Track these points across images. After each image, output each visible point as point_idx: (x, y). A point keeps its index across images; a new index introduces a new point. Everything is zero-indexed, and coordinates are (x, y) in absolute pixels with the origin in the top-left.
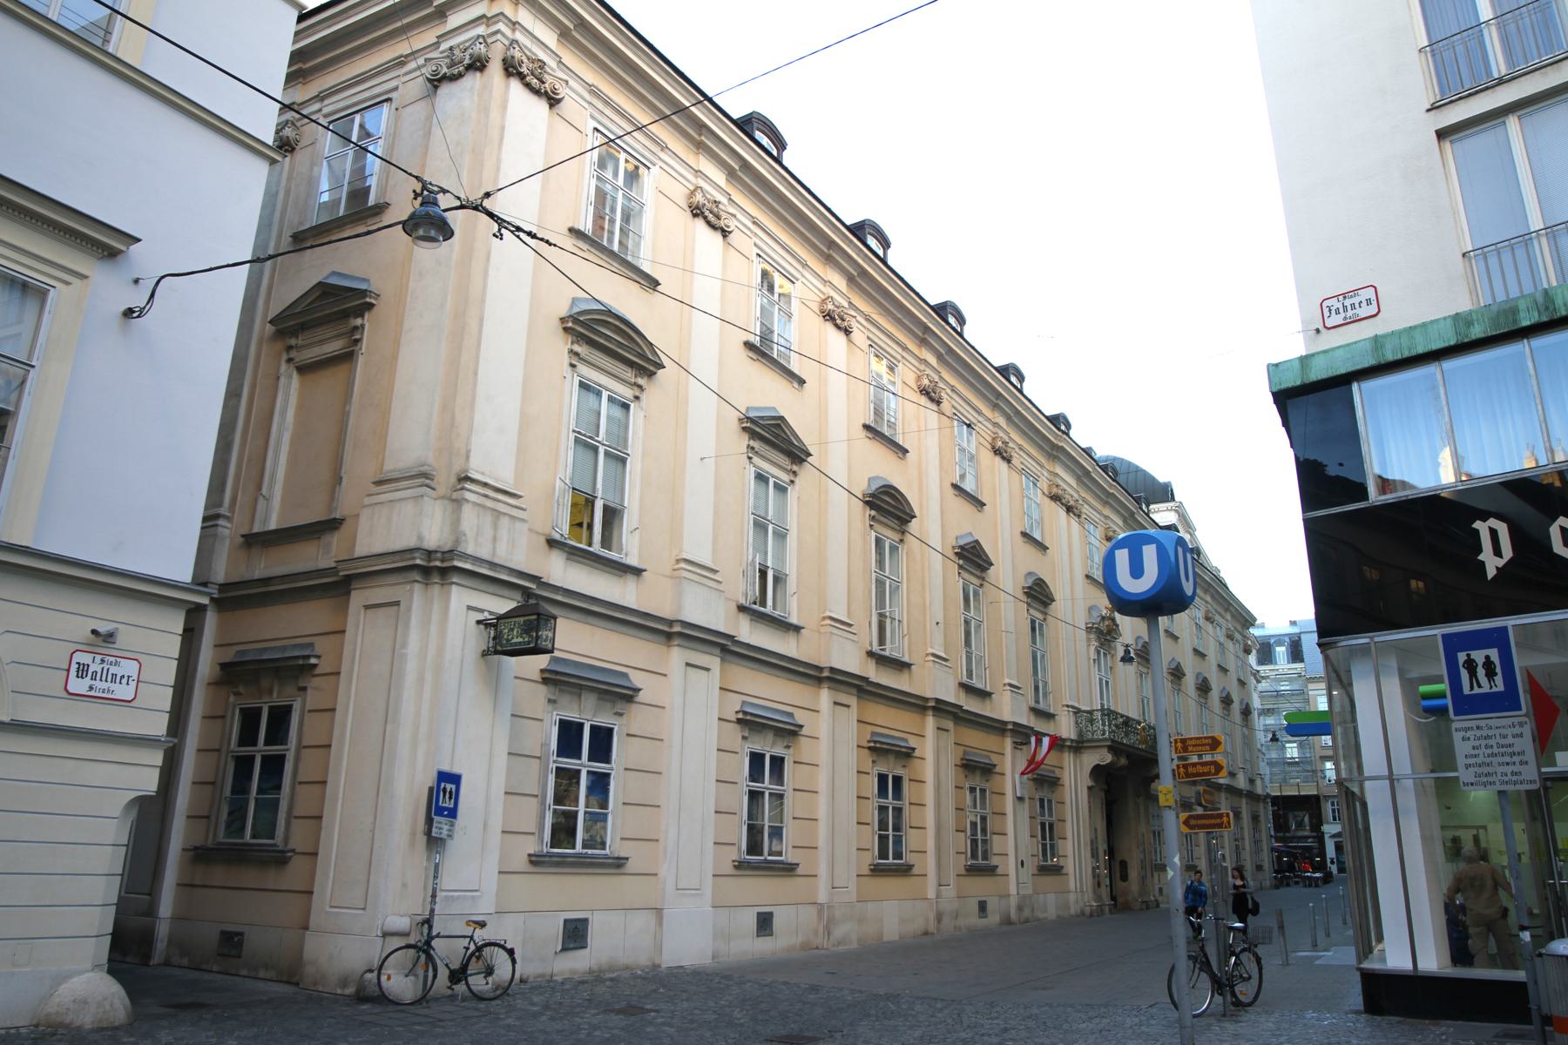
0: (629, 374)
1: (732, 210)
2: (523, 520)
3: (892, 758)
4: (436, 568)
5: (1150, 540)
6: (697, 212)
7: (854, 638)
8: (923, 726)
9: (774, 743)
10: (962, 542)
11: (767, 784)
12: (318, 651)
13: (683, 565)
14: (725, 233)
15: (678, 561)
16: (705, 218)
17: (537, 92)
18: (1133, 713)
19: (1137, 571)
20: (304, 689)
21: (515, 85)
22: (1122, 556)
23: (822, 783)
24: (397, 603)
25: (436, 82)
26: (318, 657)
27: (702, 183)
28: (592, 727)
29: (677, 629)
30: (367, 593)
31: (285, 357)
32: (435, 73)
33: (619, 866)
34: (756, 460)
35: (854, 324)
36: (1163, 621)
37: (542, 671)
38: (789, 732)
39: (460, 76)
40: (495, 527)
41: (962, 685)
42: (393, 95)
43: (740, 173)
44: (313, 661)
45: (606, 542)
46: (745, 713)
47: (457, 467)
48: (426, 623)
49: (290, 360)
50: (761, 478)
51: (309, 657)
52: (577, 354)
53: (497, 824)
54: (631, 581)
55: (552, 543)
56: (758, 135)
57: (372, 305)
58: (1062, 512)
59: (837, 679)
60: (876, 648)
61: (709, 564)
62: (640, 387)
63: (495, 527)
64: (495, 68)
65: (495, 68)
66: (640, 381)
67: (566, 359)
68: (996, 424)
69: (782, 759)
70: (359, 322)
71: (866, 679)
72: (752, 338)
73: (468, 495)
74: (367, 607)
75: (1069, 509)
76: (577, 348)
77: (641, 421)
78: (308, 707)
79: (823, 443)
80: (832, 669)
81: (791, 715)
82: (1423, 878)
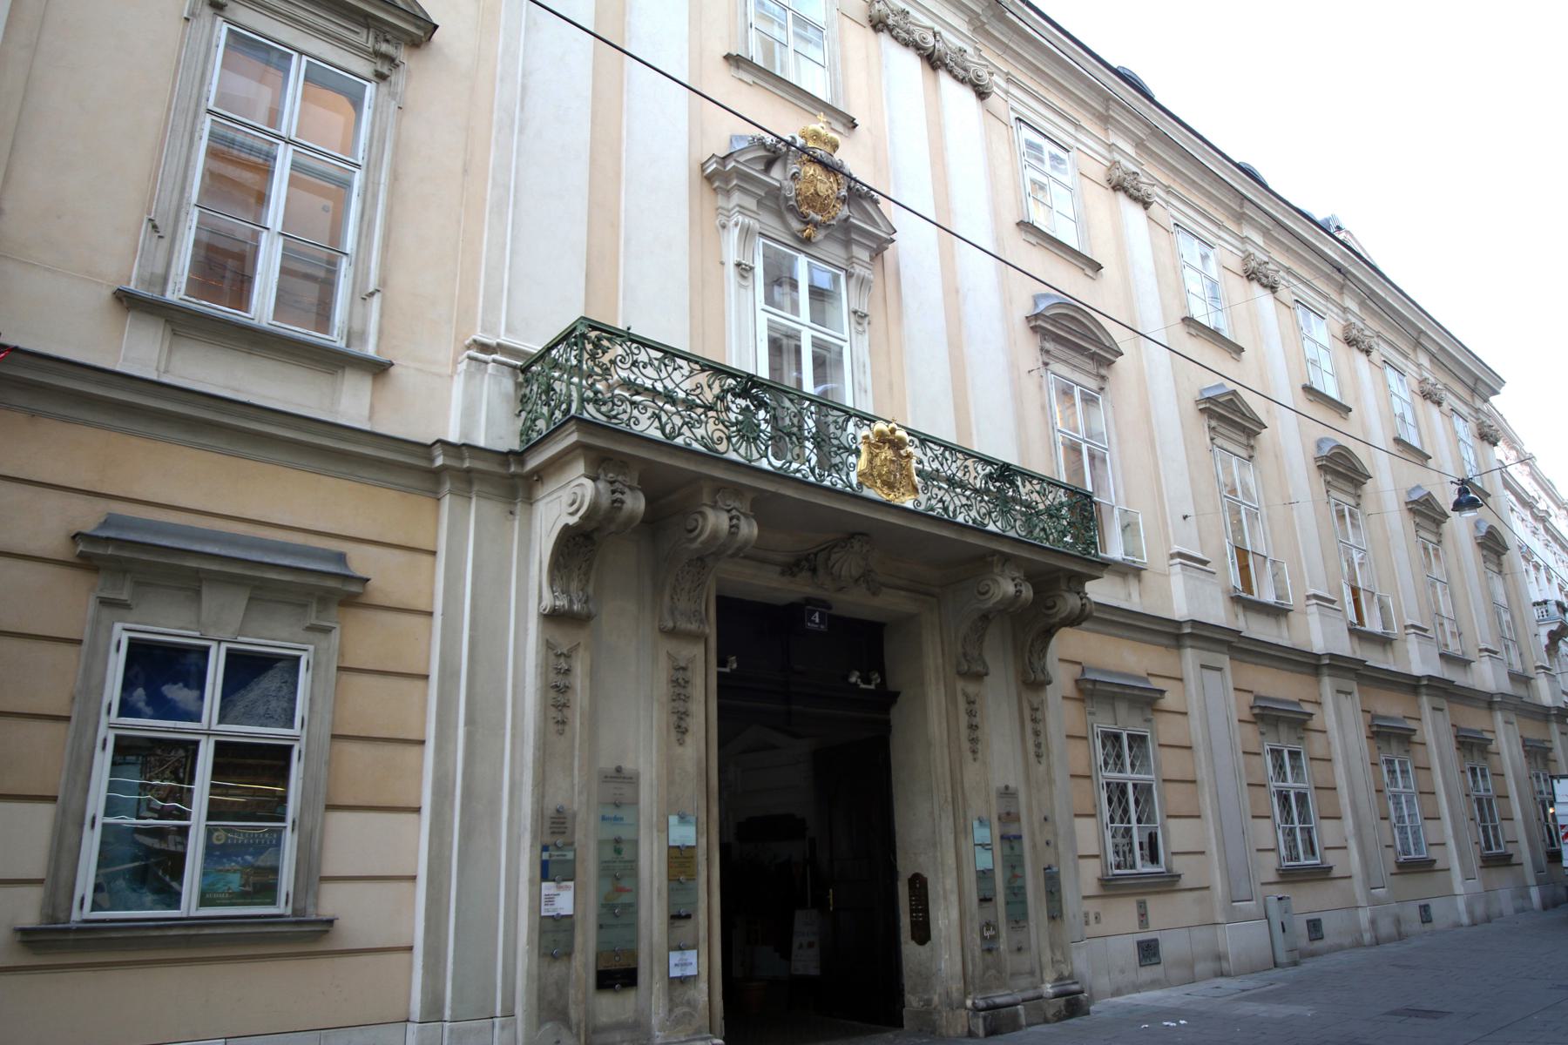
3: (1283, 729)
6: (1117, 187)
17: (962, 81)
28: (231, 654)
37: (77, 537)
52: (1048, 352)
58: (910, 62)
62: (390, 60)
66: (384, 47)
68: (1244, 239)
69: (1143, 738)
75: (933, 61)
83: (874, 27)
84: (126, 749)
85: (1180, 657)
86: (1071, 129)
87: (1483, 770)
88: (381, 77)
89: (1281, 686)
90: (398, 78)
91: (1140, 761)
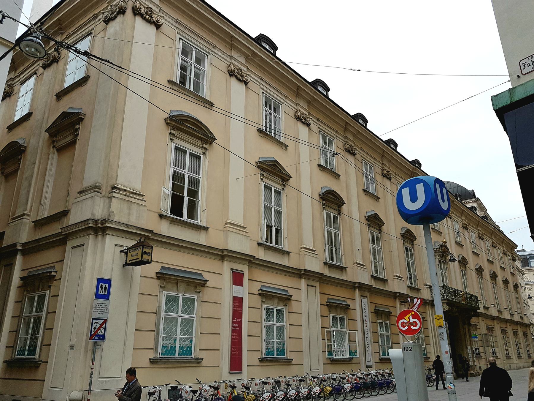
0: (200, 143)
1: (249, 73)
2: (145, 206)
4: (99, 228)
5: (420, 181)
6: (232, 74)
7: (317, 256)
8: (396, 304)
9: (278, 303)
10: (369, 214)
11: (179, 314)
12: (56, 269)
13: (303, 249)
14: (246, 83)
15: (301, 248)
16: (236, 76)
17: (150, 22)
18: (460, 288)
19: (414, 198)
20: (50, 287)
21: (138, 19)
22: (406, 192)
23: (304, 323)
24: (83, 245)
25: (107, 21)
26: (56, 272)
27: (233, 61)
29: (225, 253)
30: (73, 241)
31: (52, 145)
32: (106, 18)
33: (199, 363)
34: (265, 180)
35: (311, 121)
36: (431, 226)
38: (286, 299)
39: (115, 17)
40: (129, 209)
41: (409, 287)
42: (93, 31)
43: (251, 57)
44: (53, 273)
45: (192, 214)
46: (262, 290)
47: (112, 183)
48: (95, 253)
49: (54, 147)
50: (268, 188)
51: (51, 272)
53: (131, 344)
54: (203, 233)
55: (259, 244)
56: (264, 45)
57: (83, 119)
59: (361, 287)
60: (374, 274)
61: (242, 225)
62: (205, 148)
63: (129, 209)
64: (129, 12)
65: (129, 12)
66: (205, 146)
67: (168, 137)
70: (77, 127)
71: (253, 257)
72: (261, 127)
73: (115, 195)
74: (73, 248)
76: (173, 132)
77: (206, 163)
78: (51, 295)
79: (298, 171)
80: (305, 270)
81: (286, 291)
82: (9, 301)
83: (231, 76)
84: (166, 319)
85: (354, 292)
86: (182, 29)
87: (386, 324)
88: (204, 153)
89: (339, 294)
90: (208, 153)
91: (342, 325)
